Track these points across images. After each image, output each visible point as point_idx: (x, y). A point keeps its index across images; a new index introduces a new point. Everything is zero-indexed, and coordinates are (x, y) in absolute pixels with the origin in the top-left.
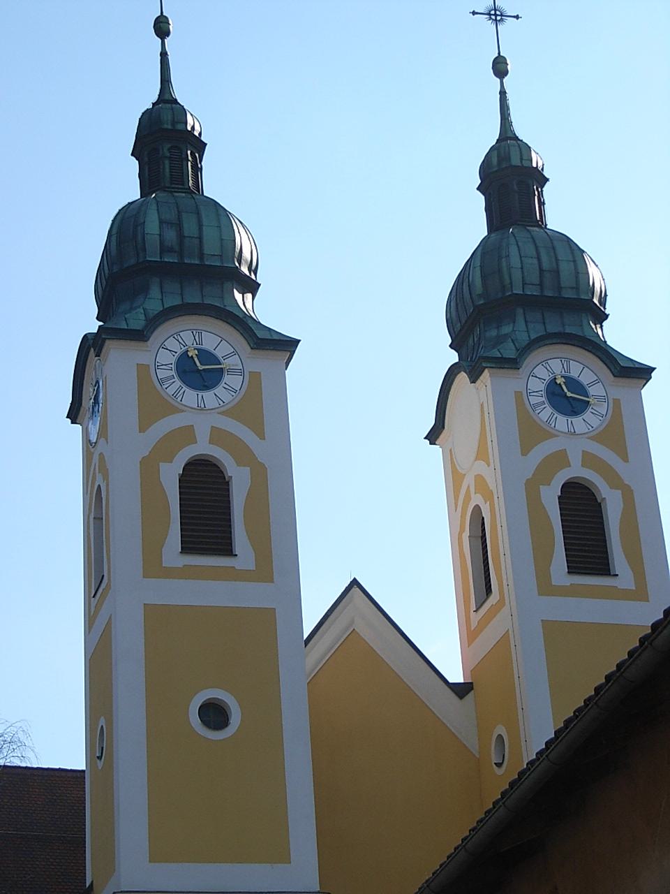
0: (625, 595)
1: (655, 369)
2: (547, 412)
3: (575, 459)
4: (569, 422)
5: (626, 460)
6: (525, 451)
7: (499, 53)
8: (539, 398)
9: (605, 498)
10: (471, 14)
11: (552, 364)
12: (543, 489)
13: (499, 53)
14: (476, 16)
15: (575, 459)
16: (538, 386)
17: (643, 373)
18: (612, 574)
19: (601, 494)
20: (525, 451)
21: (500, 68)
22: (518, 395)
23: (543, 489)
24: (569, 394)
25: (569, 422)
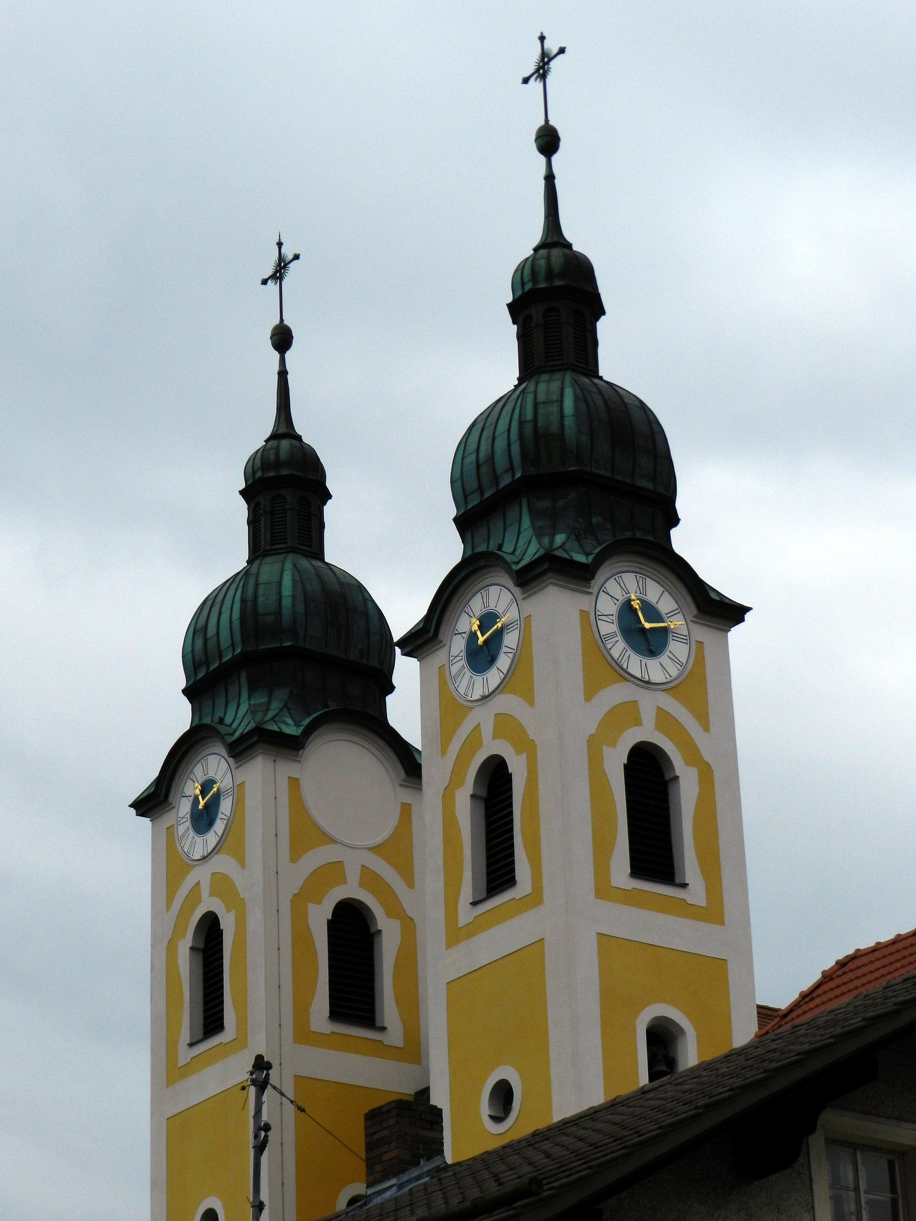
0: (382, 1051)
1: (749, 609)
2: (618, 647)
3: (353, 875)
4: (643, 665)
5: (707, 728)
6: (296, 855)
7: (547, 120)
8: (608, 627)
9: (380, 931)
10: (539, 34)
11: (625, 585)
12: (607, 751)
13: (547, 120)
14: (539, 42)
15: (353, 875)
16: (608, 606)
17: (730, 613)
18: (677, 881)
19: (376, 924)
20: (296, 855)
21: (282, 339)
22: (584, 614)
23: (607, 751)
24: (648, 625)
25: (643, 665)
